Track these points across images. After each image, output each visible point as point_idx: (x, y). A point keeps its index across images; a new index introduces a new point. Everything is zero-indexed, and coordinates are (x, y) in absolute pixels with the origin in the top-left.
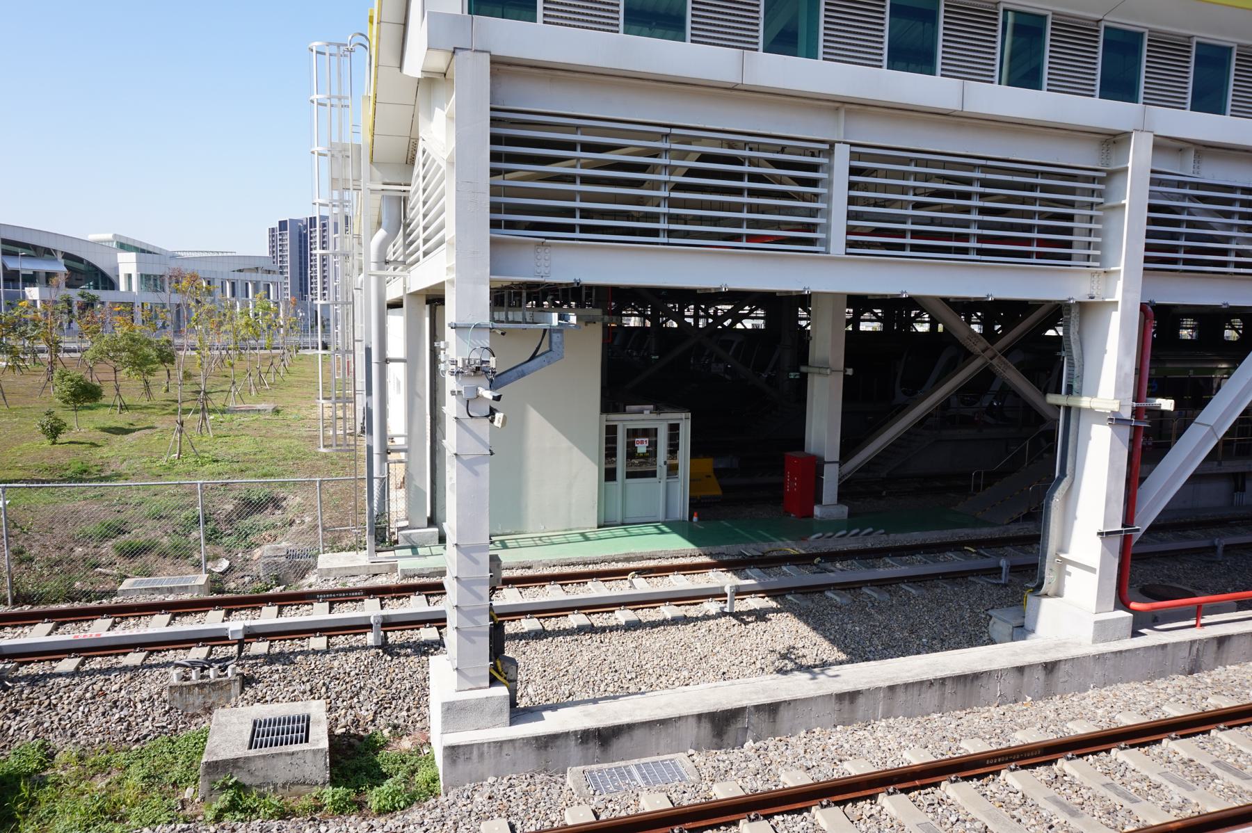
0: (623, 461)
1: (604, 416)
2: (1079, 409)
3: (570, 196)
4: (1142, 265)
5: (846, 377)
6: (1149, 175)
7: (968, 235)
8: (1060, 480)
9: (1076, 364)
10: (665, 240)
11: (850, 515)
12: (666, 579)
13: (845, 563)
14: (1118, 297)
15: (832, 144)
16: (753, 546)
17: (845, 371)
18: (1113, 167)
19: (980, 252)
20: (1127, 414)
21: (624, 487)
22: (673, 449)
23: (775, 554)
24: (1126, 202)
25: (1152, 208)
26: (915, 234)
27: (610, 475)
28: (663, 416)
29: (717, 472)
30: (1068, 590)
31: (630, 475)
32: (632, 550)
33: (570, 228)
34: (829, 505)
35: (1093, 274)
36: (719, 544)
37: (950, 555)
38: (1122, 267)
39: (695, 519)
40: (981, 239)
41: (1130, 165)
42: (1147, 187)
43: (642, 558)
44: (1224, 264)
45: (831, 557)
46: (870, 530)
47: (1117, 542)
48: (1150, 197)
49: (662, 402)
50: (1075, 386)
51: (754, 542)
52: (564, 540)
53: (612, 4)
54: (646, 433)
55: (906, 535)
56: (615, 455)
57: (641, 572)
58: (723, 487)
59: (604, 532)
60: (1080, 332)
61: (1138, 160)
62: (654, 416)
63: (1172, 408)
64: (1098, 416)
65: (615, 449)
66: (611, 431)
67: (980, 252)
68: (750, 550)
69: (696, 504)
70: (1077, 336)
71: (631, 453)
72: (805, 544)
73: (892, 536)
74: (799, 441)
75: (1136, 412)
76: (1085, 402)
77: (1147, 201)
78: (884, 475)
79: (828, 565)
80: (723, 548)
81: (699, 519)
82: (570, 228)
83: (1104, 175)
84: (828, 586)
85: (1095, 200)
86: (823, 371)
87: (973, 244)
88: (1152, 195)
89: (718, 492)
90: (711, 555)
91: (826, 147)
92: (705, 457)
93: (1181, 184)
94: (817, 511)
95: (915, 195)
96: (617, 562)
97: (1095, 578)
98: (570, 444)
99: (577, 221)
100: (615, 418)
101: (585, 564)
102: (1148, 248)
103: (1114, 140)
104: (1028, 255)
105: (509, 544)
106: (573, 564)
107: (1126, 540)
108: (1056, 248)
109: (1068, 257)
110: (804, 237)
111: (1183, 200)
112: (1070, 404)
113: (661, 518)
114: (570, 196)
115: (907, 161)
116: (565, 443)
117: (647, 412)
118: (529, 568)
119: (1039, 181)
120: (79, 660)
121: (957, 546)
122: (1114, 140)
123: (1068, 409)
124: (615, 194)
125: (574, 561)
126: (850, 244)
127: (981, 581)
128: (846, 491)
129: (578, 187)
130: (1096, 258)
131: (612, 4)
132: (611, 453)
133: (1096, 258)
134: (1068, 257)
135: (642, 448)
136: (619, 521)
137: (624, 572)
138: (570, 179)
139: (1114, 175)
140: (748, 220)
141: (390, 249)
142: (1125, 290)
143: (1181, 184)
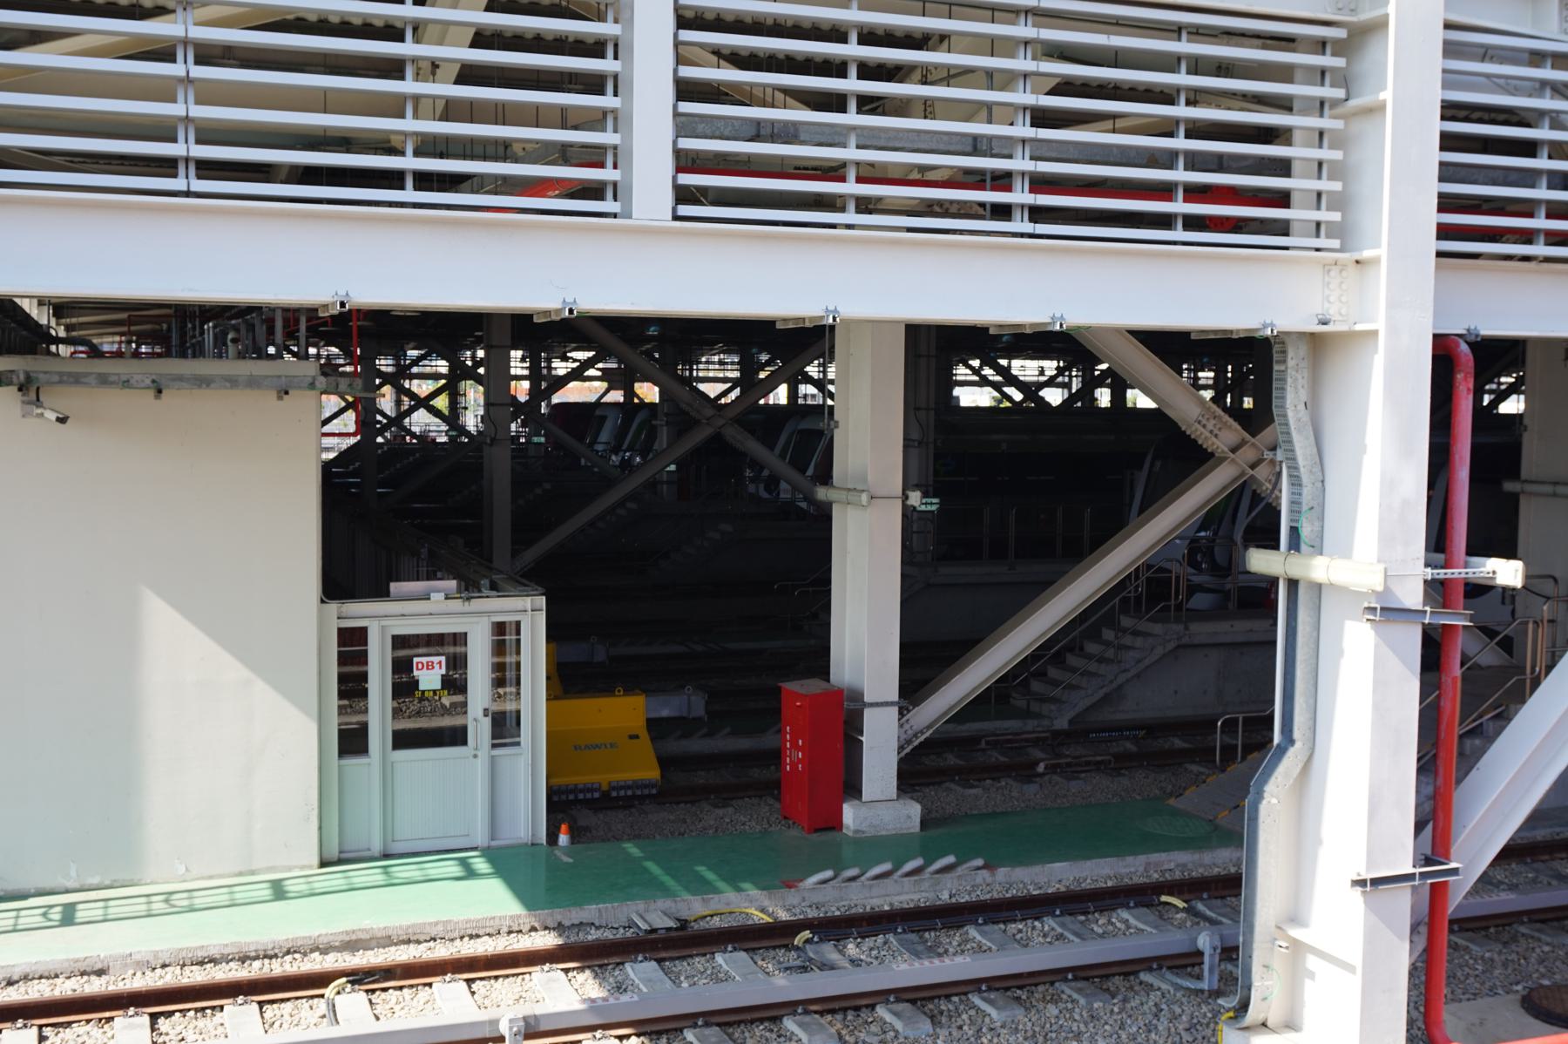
0: (381, 708)
1: (333, 607)
2: (1318, 588)
3: (1528, 178)
4: (1432, 244)
5: (908, 514)
6: (1439, 34)
7: (1008, 175)
8: (1282, 750)
9: (1305, 478)
10: (1028, 227)
11: (924, 824)
12: (424, 993)
13: (869, 942)
14: (1380, 325)
16: (664, 903)
17: (905, 497)
18: (1365, 16)
20: (1412, 596)
21: (385, 765)
22: (505, 676)
23: (716, 922)
24: (1387, 95)
25: (1451, 111)
26: (1196, 193)
27: (353, 742)
28: (477, 604)
29: (656, 727)
30: (1311, 1014)
31: (403, 740)
32: (42, 958)
33: (1165, 221)
34: (879, 803)
35: (1327, 267)
36: (578, 903)
37: (1124, 915)
38: (1382, 252)
39: (563, 839)
40: (1040, 183)
41: (1391, 9)
42: (1436, 61)
43: (387, 941)
45: (835, 928)
46: (951, 859)
47: (1402, 903)
48: (1446, 85)
49: (474, 578)
50: (1306, 532)
51: (666, 892)
52: (223, 897)
54: (434, 642)
55: (1037, 869)
56: (364, 694)
57: (359, 977)
58: (665, 762)
59: (334, 877)
60: (1313, 406)
62: (456, 605)
65: (364, 677)
66: (352, 642)
68: (655, 915)
69: (565, 804)
70: (1304, 415)
71: (404, 687)
72: (792, 897)
73: (1002, 873)
74: (818, 659)
75: (1437, 591)
76: (1318, 569)
77: (1436, 95)
78: (1062, 723)
79: (829, 952)
80: (589, 912)
81: (574, 839)
82: (1165, 221)
83: (1341, 33)
84: (882, 995)
85: (1326, 92)
86: (852, 497)
88: (1450, 79)
89: (653, 774)
90: (560, 928)
92: (628, 691)
93: (1537, 58)
94: (849, 814)
96: (325, 951)
97: (1355, 981)
98: (245, 673)
100: (360, 612)
101: (243, 959)
102: (1447, 203)
105: (291, 887)
106: (214, 961)
107: (1438, 893)
109: (1283, 228)
111: (1540, 95)
112: (1294, 572)
113: (481, 838)
116: (232, 670)
117: (437, 597)
118: (100, 973)
121: (1142, 895)
123: (1293, 584)
124: (325, 91)
125: (214, 952)
126: (684, 195)
127: (1163, 982)
128: (915, 772)
130: (1337, 231)
132: (352, 687)
133: (1337, 231)
134: (1283, 228)
135: (429, 676)
136: (377, 847)
137: (320, 980)
142: (1391, 305)
143: (1537, 58)
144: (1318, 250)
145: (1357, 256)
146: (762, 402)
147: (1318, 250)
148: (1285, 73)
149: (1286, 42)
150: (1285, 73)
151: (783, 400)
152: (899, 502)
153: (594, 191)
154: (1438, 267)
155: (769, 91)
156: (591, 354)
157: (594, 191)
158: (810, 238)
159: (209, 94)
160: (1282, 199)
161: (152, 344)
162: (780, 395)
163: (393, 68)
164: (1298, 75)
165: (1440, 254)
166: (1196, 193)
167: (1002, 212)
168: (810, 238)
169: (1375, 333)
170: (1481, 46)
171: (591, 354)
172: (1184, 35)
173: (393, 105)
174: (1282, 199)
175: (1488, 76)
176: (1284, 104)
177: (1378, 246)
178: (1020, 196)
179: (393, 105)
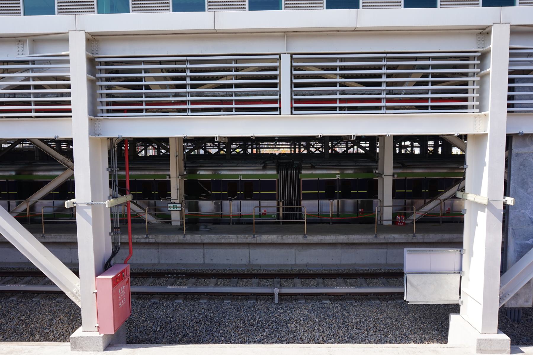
3: (28, 95)
10: (384, 112)
14: (488, 132)
15: (280, 55)
19: (193, 110)
26: (434, 100)
40: (193, 103)
42: (507, 59)
44: (30, 111)
53: (397, 2)
61: (499, 46)
63: (512, 204)
64: (480, 206)
91: (278, 57)
103: (484, 33)
104: (334, 109)
108: (455, 101)
109: (465, 107)
110: (272, 107)
114: (28, 95)
115: (335, 60)
119: (431, 62)
122: (484, 33)
129: (32, 91)
131: (397, 2)
138: (230, 86)
139: (484, 56)
140: (340, 99)
146: (192, 153)
148: (466, 66)
149: (467, 58)
150: (466, 66)
151: (352, 152)
153: (275, 109)
154: (507, 115)
156: (18, 146)
157: (275, 109)
158: (164, 119)
160: (465, 100)
161: (199, 155)
162: (143, 153)
163: (140, 87)
164: (470, 66)
165: (508, 112)
166: (238, 102)
169: (487, 134)
170: (527, 53)
171: (18, 146)
172: (431, 59)
173: (140, 95)
174: (465, 100)
175: (530, 61)
176: (466, 75)
178: (383, 104)
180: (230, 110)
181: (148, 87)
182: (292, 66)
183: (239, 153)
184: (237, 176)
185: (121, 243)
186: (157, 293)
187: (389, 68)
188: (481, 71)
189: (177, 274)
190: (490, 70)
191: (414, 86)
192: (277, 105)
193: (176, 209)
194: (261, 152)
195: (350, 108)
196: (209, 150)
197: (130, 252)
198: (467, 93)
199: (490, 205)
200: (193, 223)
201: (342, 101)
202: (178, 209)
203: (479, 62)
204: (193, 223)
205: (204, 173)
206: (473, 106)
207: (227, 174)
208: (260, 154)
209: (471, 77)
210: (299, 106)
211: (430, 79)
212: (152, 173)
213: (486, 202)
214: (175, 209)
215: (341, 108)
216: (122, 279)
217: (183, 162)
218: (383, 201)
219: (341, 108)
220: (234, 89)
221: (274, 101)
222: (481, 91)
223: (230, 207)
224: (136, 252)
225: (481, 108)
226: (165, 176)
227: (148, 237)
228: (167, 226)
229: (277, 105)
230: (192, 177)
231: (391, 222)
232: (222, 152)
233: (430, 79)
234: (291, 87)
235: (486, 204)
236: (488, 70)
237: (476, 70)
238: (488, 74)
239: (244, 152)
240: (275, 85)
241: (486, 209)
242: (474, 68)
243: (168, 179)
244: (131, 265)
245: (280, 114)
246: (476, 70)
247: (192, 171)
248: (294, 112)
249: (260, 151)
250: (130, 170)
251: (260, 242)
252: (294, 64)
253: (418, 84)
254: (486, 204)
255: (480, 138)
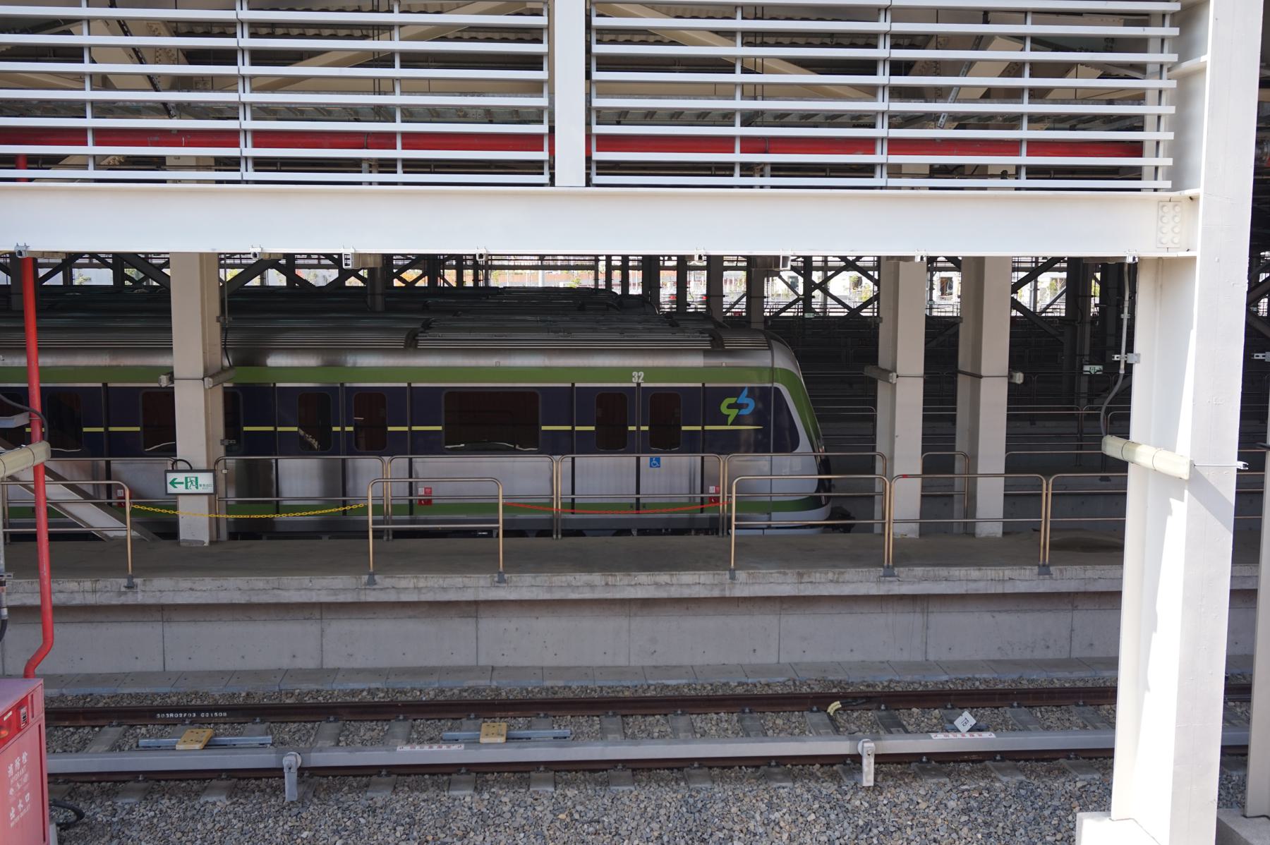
5: (1012, 387)
7: (235, 133)
11: (1004, 533)
17: (1010, 377)
19: (261, 164)
26: (412, 140)
33: (726, 169)
40: (261, 138)
59: (242, 546)
64: (1170, 484)
67: (261, 164)
87: (248, 150)
95: (253, 35)
99: (89, 122)
108: (1105, 155)
109: (1135, 173)
120: (121, 729)
134: (1135, 173)
141: (846, 278)
144: (1156, 190)
145: (1188, 193)
147: (1156, 190)
148: (1139, 45)
150: (1139, 45)
152: (1006, 381)
153: (536, 167)
155: (759, 61)
157: (536, 167)
158: (496, 194)
159: (410, 87)
160: (1136, 149)
161: (265, 290)
166: (412, 140)
167: (232, 164)
168: (996, 198)
169: (1194, 259)
174: (1136, 149)
177: (1198, 187)
179: (725, 91)
180: (387, 166)
181: (104, 82)
182: (589, 109)
183: (410, 285)
184: (627, 372)
185: (10, 609)
186: (134, 775)
187: (899, 41)
188: (1182, 59)
189: (199, 710)
190: (1206, 58)
191: (1002, 75)
192: (540, 21)
193: (193, 485)
194: (493, 284)
195: (779, 170)
196: (303, 273)
197: (45, 638)
198: (1141, 129)
199: (1196, 480)
200: (253, 529)
201: (750, 144)
202: (200, 490)
203: (1175, 31)
204: (253, 529)
205: (290, 365)
206: (1157, 168)
207: (375, 365)
208: (487, 288)
209: (1153, 76)
210: (622, 156)
211: (1026, 81)
212: (103, 360)
213: (1184, 472)
214: (193, 490)
215: (748, 169)
216: (19, 730)
217: (217, 327)
218: (892, 458)
219: (748, 169)
220: (397, 72)
221: (533, 142)
222: (1181, 124)
223: (377, 480)
224: (64, 633)
225: (1178, 176)
226: (156, 371)
227: (131, 587)
228: (165, 546)
229: (543, 155)
230: (249, 376)
231: (916, 527)
232: (352, 282)
233: (1026, 81)
234: (588, 124)
235: (1186, 477)
236: (1203, 59)
237: (1169, 57)
238: (1201, 71)
239: (433, 281)
240: (534, 62)
241: (1186, 492)
242: (1162, 52)
243: (164, 382)
244: (50, 680)
245: (552, 182)
246: (1169, 57)
247: (249, 356)
248: (596, 179)
249: (487, 279)
250: (42, 350)
251: (1087, 654)
252: (597, 102)
253: (989, 94)
254: (1186, 477)
255: (1173, 269)
